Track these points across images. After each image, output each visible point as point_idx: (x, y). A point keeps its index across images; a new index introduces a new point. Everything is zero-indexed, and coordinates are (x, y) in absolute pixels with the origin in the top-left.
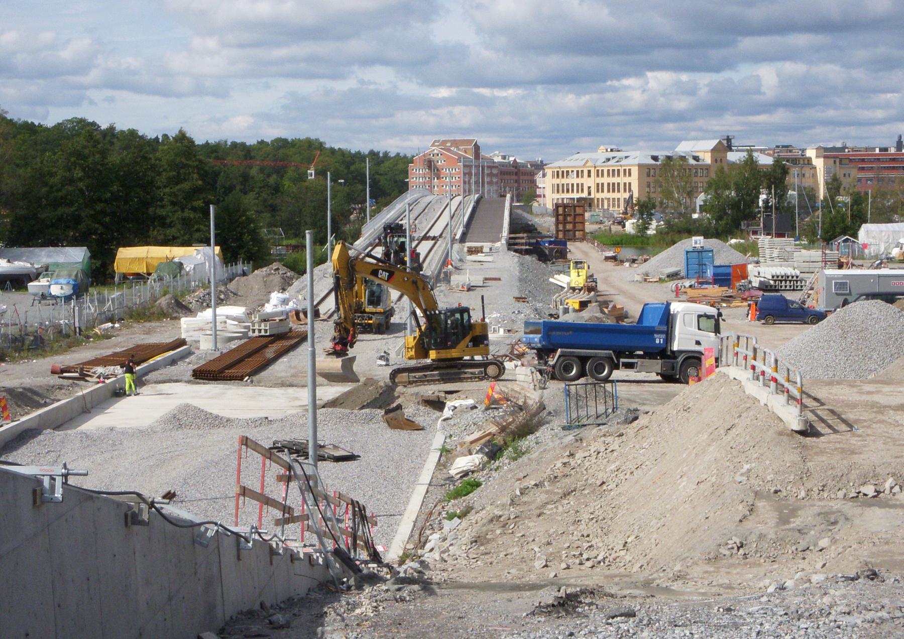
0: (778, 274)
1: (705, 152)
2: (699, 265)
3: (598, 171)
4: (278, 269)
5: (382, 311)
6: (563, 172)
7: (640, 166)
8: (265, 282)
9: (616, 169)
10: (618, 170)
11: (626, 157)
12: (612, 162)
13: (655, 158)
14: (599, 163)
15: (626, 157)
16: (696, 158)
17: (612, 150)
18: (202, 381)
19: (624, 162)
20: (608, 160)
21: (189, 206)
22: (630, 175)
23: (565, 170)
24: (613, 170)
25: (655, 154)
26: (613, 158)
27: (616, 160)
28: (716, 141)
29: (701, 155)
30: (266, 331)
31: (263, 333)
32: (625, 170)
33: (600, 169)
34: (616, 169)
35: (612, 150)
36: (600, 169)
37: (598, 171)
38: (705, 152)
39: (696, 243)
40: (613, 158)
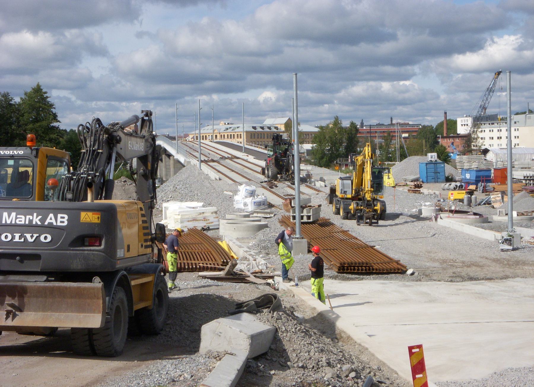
0: (528, 175)
1: (281, 124)
2: (435, 173)
3: (221, 136)
4: (125, 181)
5: (351, 197)
6: (203, 136)
7: (247, 132)
8: (124, 190)
9: (232, 134)
10: (234, 135)
11: (238, 127)
12: (229, 130)
13: (254, 128)
14: (222, 131)
15: (238, 127)
16: (276, 128)
17: (228, 124)
18: (350, 276)
19: (237, 130)
20: (227, 129)
21: (47, 138)
22: (241, 137)
23: (204, 135)
24: (231, 135)
25: (254, 125)
26: (230, 128)
27: (231, 129)
28: (287, 119)
29: (279, 126)
30: (309, 217)
31: (305, 220)
32: (238, 135)
33: (223, 134)
34: (232, 134)
35: (228, 124)
36: (223, 134)
37: (221, 136)
38: (281, 124)
39: (432, 157)
40: (230, 128)
